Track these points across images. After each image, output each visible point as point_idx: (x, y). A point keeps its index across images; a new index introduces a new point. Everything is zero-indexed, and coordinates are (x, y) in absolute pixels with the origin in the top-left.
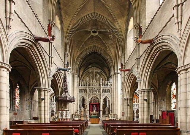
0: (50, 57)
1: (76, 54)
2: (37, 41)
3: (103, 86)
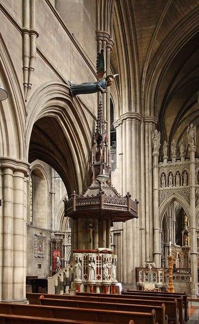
0: (23, 32)
1: (149, 45)
2: (75, 95)
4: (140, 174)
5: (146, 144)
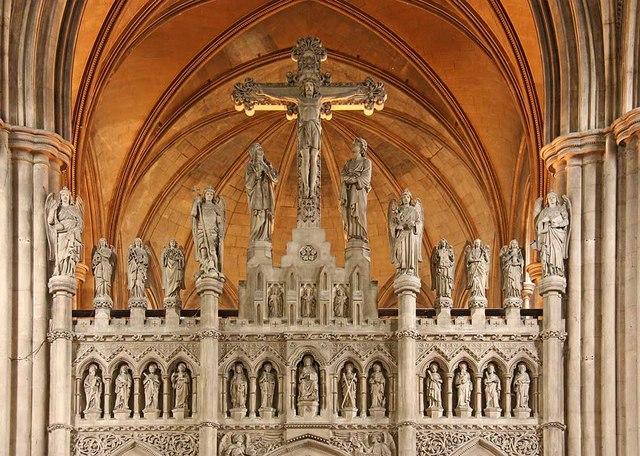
3: (427, 312)
5: (23, 242)
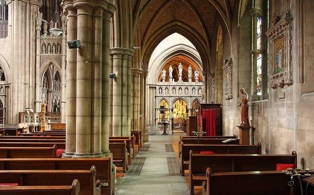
4: (25, 42)
5: (31, 21)
